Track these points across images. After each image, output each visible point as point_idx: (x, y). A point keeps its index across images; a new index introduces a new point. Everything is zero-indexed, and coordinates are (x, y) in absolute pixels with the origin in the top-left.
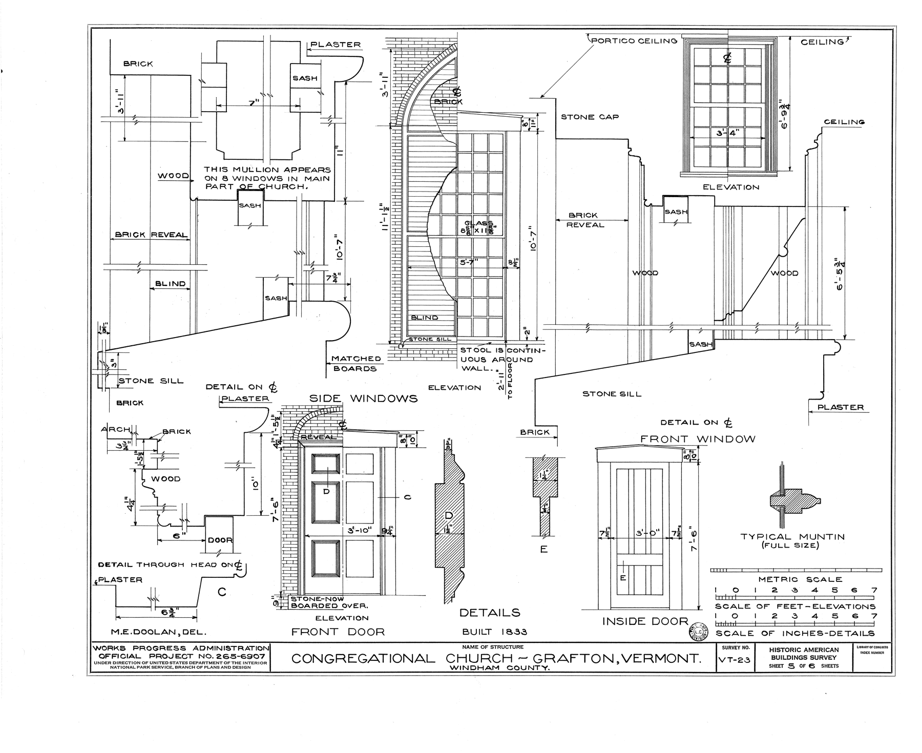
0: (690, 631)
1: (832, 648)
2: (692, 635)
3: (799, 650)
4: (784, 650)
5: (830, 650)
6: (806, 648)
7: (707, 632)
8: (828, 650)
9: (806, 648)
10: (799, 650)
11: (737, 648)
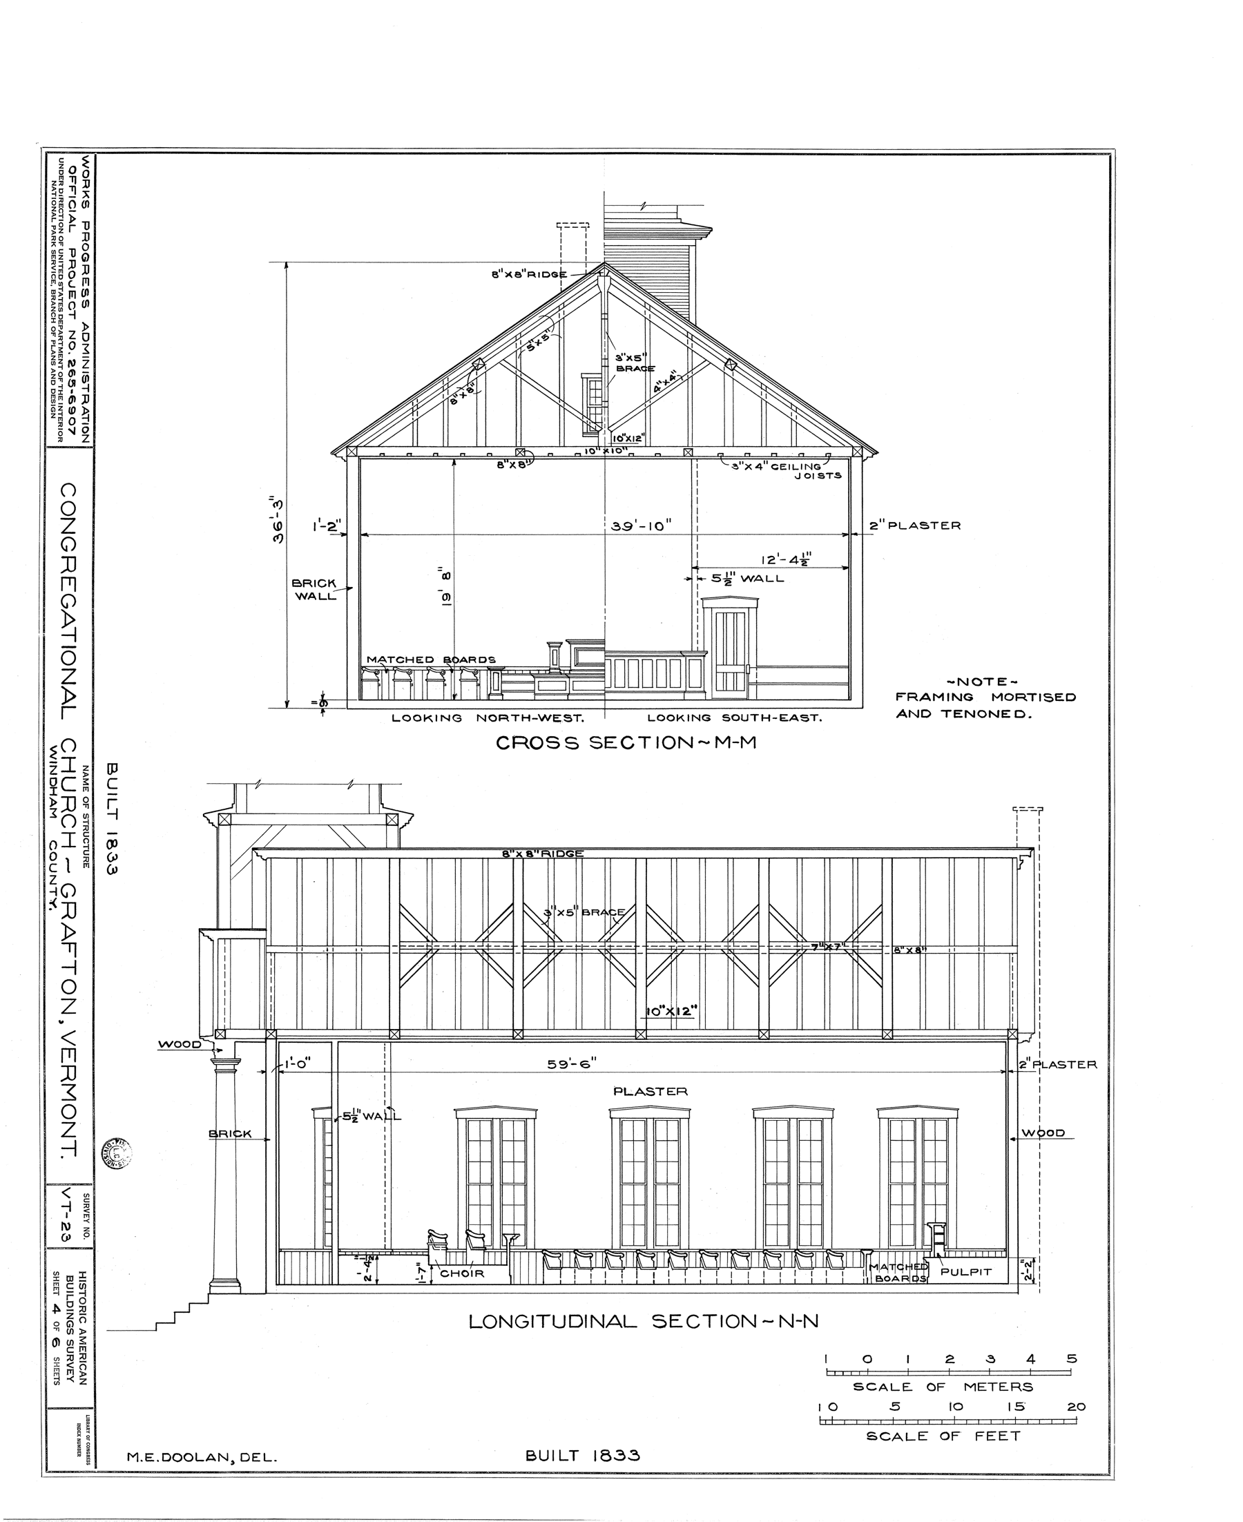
0: (117, 1140)
2: (111, 1143)
11: (86, 1219)
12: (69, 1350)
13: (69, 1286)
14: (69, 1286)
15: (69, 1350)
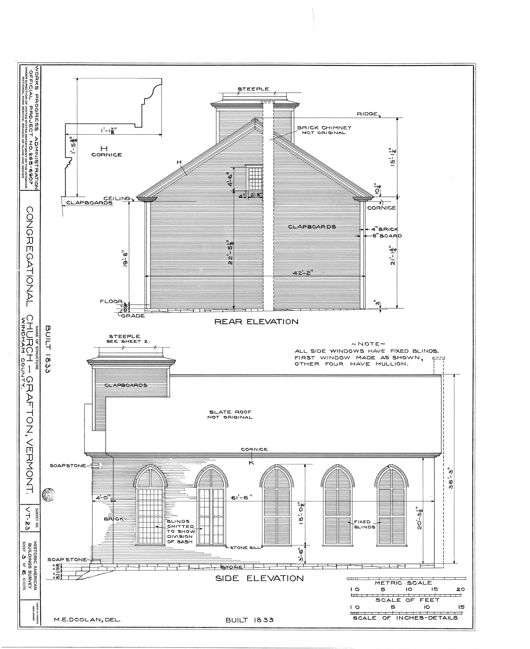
0: (49, 489)
1: (36, 585)
3: (35, 562)
4: (35, 552)
5: (35, 584)
6: (36, 567)
7: (49, 500)
8: (35, 582)
9: (36, 567)
10: (35, 562)
11: (37, 519)
12: (30, 575)
13: (29, 548)
14: (29, 548)
15: (30, 575)
